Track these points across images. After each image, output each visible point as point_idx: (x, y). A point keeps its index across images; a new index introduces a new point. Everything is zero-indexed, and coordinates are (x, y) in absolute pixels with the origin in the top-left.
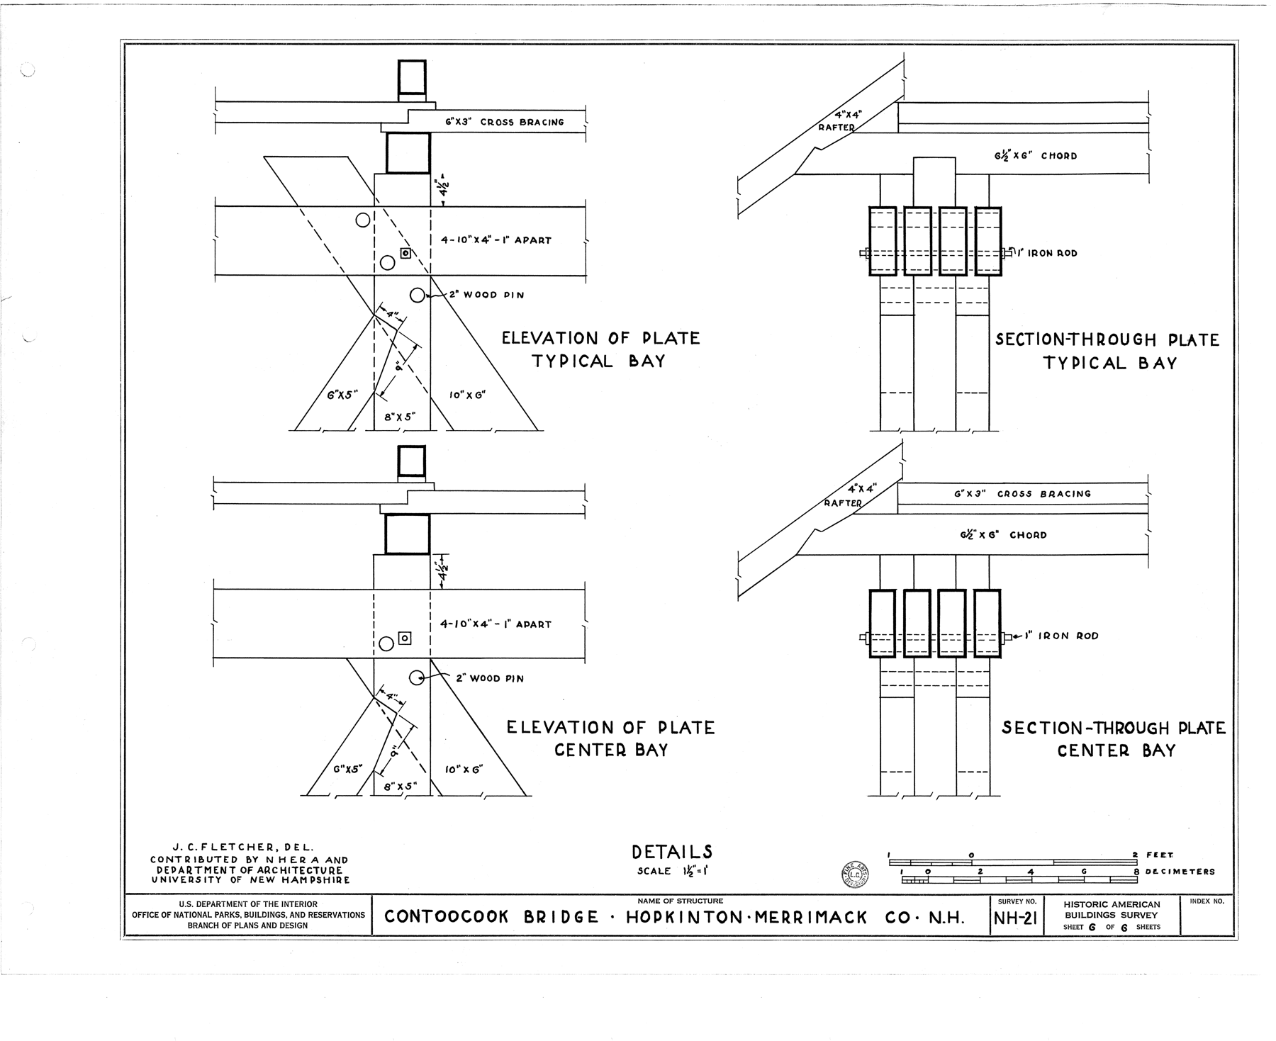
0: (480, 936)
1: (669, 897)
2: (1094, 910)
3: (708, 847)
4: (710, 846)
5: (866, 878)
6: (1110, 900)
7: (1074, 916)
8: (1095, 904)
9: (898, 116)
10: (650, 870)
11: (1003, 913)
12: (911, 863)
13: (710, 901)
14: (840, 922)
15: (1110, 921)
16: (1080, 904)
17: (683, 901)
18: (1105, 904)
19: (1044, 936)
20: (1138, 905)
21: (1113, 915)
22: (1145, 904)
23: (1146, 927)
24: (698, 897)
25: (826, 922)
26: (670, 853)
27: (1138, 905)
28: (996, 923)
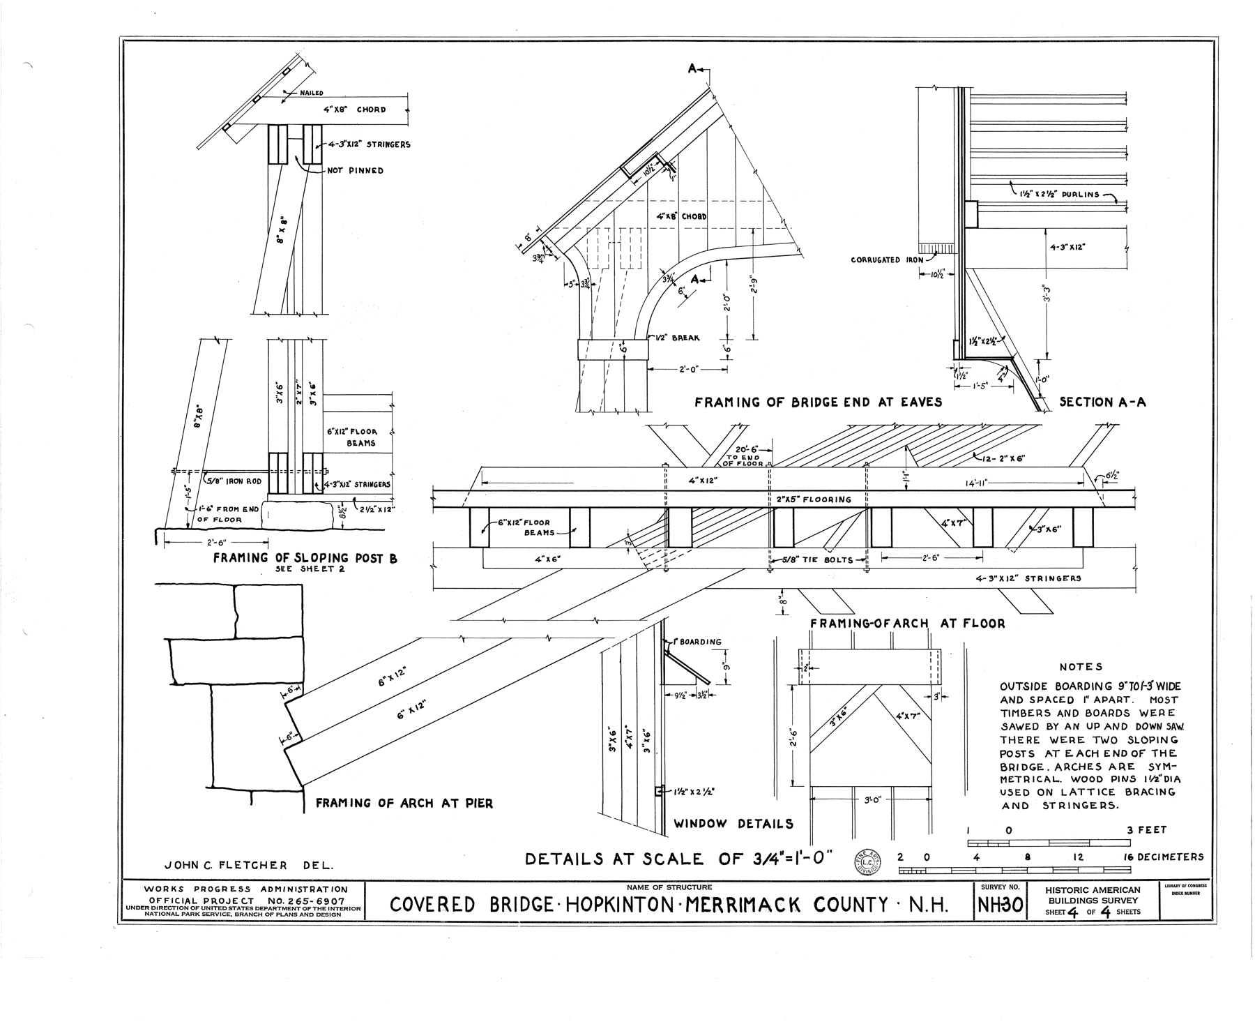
0: (476, 922)
1: (658, 884)
2: (1076, 895)
3: (598, 855)
4: (600, 854)
5: (878, 866)
6: (1091, 885)
7: (1058, 901)
8: (1077, 890)
9: (620, 662)
10: (666, 858)
11: (624, 911)
12: (988, 843)
13: (699, 887)
14: (771, 910)
15: (1092, 906)
16: (1062, 890)
17: (672, 887)
18: (1086, 890)
19: (1160, 920)
20: (1119, 891)
21: (1095, 901)
22: (1125, 890)
23: (1126, 912)
24: (687, 884)
25: (754, 911)
26: (566, 860)
27: (1119, 891)
28: (980, 911)
